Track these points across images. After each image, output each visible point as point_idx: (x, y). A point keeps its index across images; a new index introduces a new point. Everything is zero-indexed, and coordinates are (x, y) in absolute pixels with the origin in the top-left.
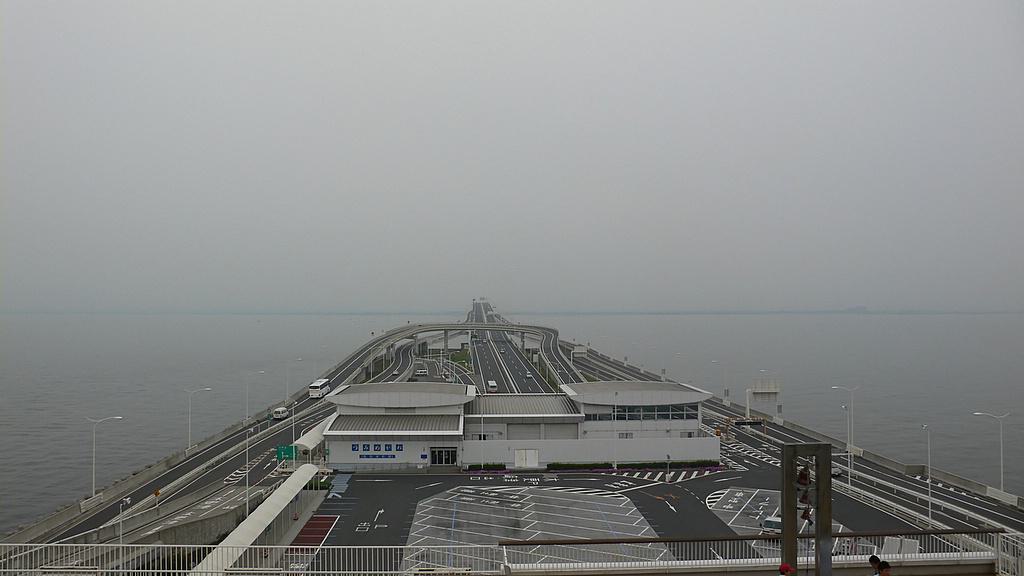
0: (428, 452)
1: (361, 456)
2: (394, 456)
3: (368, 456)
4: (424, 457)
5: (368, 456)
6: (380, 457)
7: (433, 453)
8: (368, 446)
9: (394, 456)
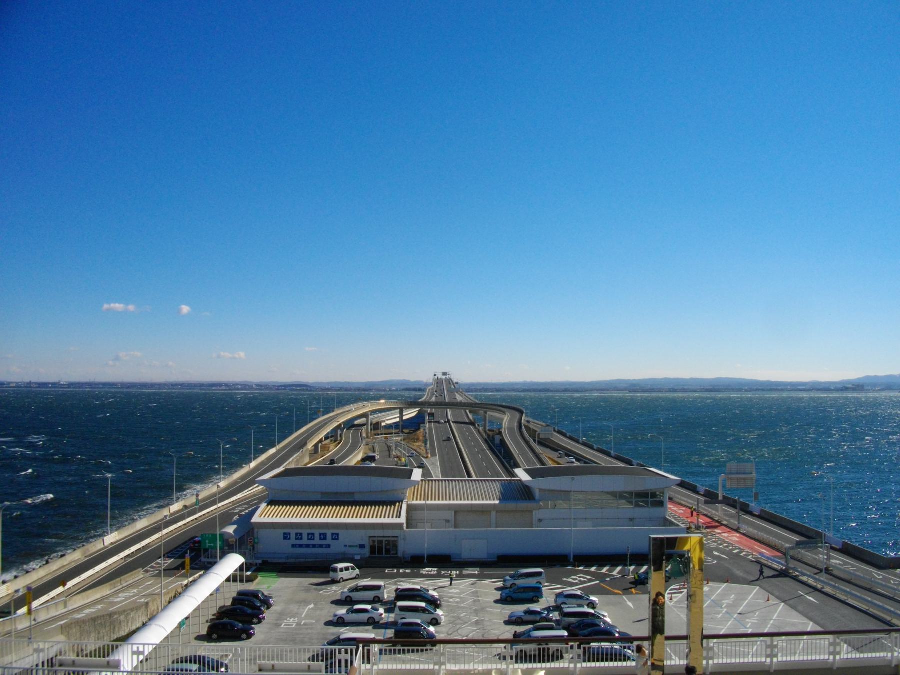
0: (366, 542)
1: (293, 546)
2: (329, 546)
3: (301, 546)
4: (362, 547)
5: (301, 546)
8: (301, 534)
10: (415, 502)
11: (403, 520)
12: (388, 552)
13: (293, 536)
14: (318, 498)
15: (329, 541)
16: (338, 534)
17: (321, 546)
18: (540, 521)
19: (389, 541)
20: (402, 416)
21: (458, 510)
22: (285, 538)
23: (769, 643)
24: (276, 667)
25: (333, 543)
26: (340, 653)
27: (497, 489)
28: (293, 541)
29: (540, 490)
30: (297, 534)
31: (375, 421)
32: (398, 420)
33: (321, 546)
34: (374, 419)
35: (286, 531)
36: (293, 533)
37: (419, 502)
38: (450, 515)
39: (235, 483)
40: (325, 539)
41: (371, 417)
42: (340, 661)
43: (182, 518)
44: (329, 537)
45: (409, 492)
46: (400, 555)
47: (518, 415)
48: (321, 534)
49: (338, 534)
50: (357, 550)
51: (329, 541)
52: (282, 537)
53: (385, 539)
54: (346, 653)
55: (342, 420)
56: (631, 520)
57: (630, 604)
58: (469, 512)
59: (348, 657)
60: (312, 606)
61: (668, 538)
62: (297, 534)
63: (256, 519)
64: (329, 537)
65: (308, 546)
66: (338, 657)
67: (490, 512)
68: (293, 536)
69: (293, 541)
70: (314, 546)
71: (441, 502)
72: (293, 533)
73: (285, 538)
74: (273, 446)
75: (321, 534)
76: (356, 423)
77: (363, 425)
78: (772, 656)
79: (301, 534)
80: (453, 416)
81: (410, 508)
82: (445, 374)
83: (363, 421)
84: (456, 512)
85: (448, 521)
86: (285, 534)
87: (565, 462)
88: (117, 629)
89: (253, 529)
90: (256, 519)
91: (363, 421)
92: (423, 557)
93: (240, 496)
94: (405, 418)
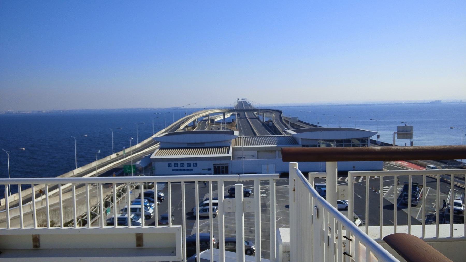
1: (173, 170)
2: (192, 170)
6: (184, 170)
7: (215, 168)
8: (177, 164)
9: (192, 170)
10: (236, 147)
11: (230, 155)
13: (173, 165)
14: (186, 146)
15: (192, 167)
16: (196, 163)
19: (223, 166)
20: (224, 117)
21: (259, 150)
22: (169, 166)
24: (43, 243)
25: (194, 168)
27: (275, 140)
28: (173, 168)
29: (302, 139)
30: (175, 164)
31: (212, 119)
32: (223, 118)
34: (212, 117)
35: (169, 163)
36: (173, 163)
37: (238, 147)
38: (255, 153)
39: (145, 145)
40: (190, 166)
41: (210, 117)
43: (117, 160)
44: (192, 165)
45: (233, 141)
47: (279, 114)
48: (187, 164)
49: (196, 163)
51: (192, 167)
52: (167, 165)
53: (221, 165)
55: (197, 117)
58: (266, 151)
61: (261, 207)
62: (175, 164)
63: (151, 157)
64: (192, 165)
67: (275, 151)
68: (173, 165)
69: (173, 168)
71: (249, 146)
72: (173, 163)
73: (169, 166)
74: (164, 128)
75: (187, 164)
76: (204, 119)
77: (206, 120)
79: (177, 164)
80: (248, 115)
81: (234, 150)
82: (242, 99)
83: (207, 118)
84: (258, 151)
85: (254, 156)
86: (168, 164)
87: (308, 127)
88: (70, 216)
89: (151, 163)
90: (151, 157)
91: (207, 118)
93: (147, 150)
94: (226, 117)
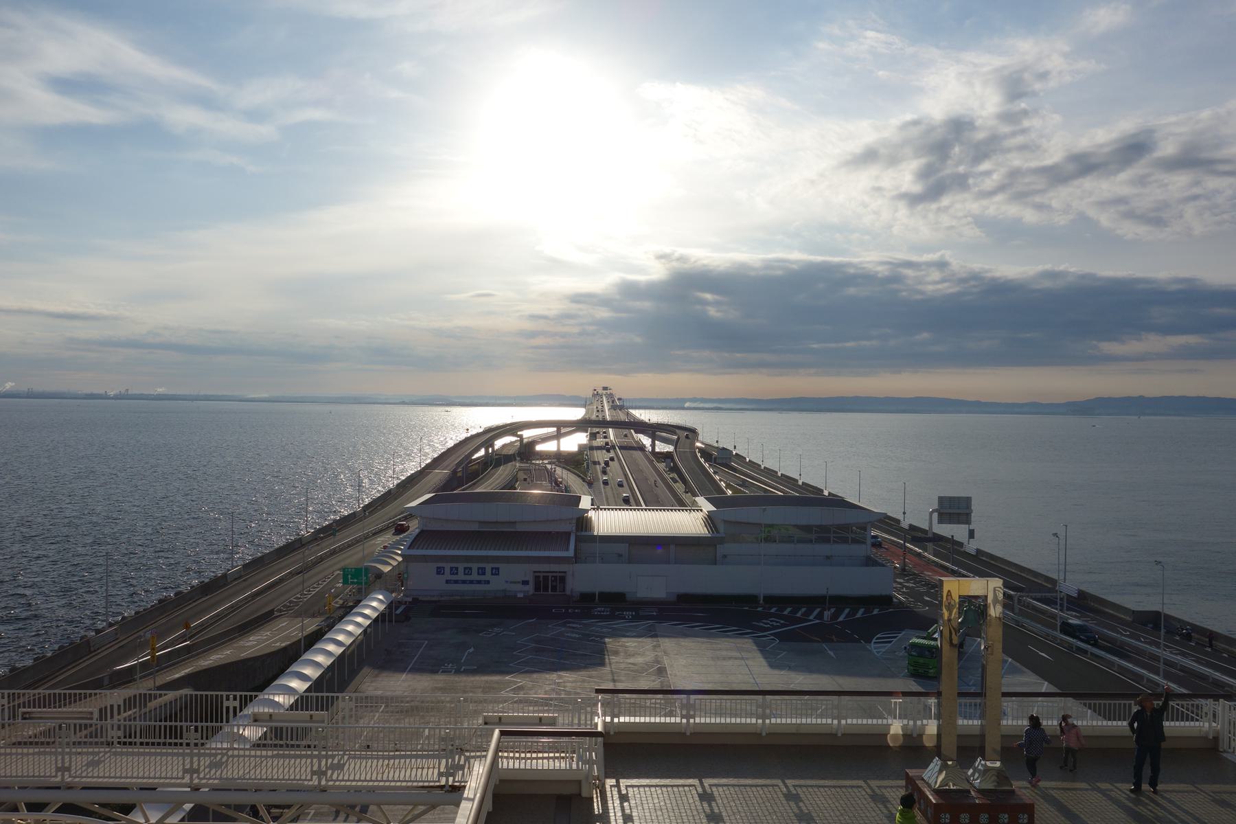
1: (448, 582)
2: (488, 582)
3: (456, 582)
4: (525, 583)
5: (456, 582)
12: (554, 588)
13: (447, 571)
15: (488, 576)
17: (479, 582)
18: (725, 556)
22: (438, 573)
23: (685, 701)
26: (228, 699)
29: (725, 522)
33: (479, 582)
40: (484, 574)
42: (228, 708)
46: (568, 592)
50: (519, 587)
51: (488, 576)
54: (235, 699)
56: (828, 557)
57: (831, 653)
59: (237, 704)
60: (472, 650)
64: (488, 571)
65: (464, 582)
66: (226, 704)
68: (447, 571)
70: (471, 582)
73: (438, 573)
78: (688, 717)
80: (616, 436)
82: (605, 388)
85: (620, 556)
92: (594, 595)
